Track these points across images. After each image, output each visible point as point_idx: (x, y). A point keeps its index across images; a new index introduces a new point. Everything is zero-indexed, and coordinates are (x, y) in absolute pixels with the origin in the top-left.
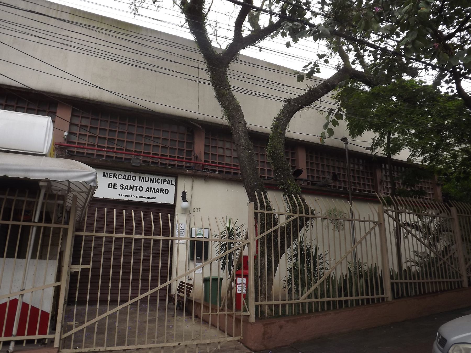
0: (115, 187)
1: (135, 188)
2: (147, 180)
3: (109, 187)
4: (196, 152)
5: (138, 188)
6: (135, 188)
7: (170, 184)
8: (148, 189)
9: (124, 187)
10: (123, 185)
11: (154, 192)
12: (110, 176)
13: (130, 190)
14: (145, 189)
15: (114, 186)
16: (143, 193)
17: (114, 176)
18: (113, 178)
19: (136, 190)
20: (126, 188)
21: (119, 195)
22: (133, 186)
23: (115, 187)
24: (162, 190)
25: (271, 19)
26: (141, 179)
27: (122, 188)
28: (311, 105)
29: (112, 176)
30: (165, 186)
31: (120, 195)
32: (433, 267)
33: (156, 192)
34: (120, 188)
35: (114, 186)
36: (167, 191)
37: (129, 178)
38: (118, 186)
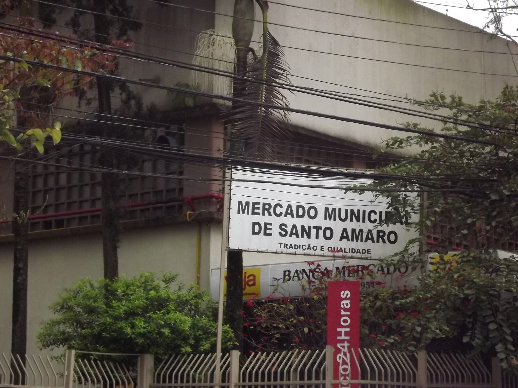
0: (268, 232)
1: (313, 232)
2: (343, 217)
3: (254, 233)
4: (429, 149)
5: (321, 232)
6: (313, 232)
7: (293, 216)
8: (372, 236)
9: (289, 229)
10: (286, 226)
11: (362, 241)
12: (256, 211)
13: (302, 237)
14: (337, 234)
15: (266, 230)
17: (264, 209)
18: (261, 213)
19: (317, 237)
20: (294, 232)
21: (281, 244)
22: (310, 227)
23: (268, 232)
24: (381, 234)
27: (283, 233)
28: (284, 105)
29: (258, 208)
31: (283, 246)
33: (366, 241)
34: (280, 234)
35: (266, 229)
37: (301, 213)
38: (275, 230)
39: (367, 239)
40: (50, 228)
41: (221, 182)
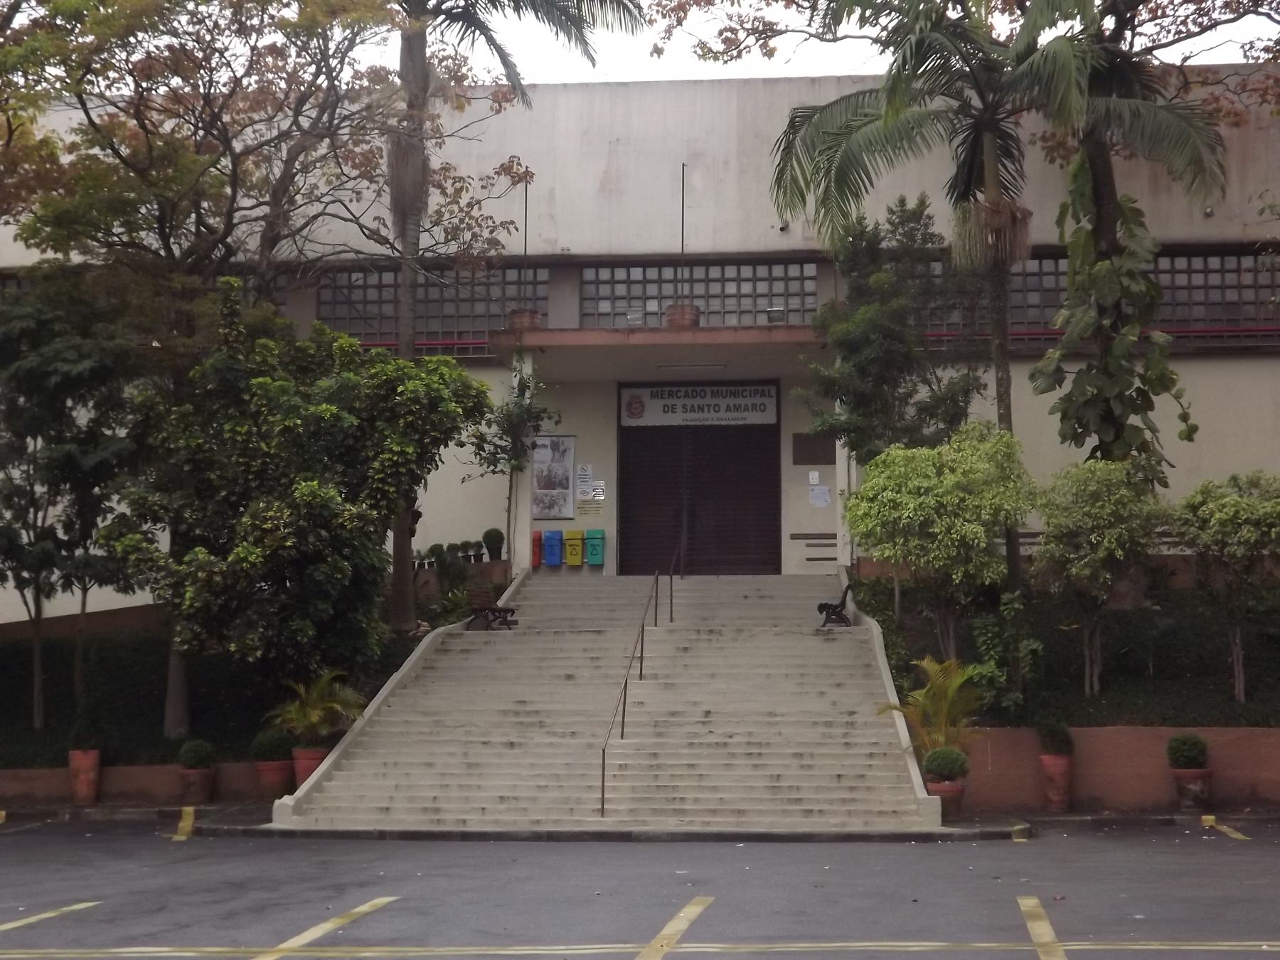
1: (706, 409)
5: (711, 408)
6: (706, 409)
9: (689, 408)
16: (722, 414)
25: (1114, 441)
26: (714, 395)
30: (758, 400)
32: (508, 810)
36: (762, 408)
39: (745, 410)
40: (753, 404)
41: (469, 287)
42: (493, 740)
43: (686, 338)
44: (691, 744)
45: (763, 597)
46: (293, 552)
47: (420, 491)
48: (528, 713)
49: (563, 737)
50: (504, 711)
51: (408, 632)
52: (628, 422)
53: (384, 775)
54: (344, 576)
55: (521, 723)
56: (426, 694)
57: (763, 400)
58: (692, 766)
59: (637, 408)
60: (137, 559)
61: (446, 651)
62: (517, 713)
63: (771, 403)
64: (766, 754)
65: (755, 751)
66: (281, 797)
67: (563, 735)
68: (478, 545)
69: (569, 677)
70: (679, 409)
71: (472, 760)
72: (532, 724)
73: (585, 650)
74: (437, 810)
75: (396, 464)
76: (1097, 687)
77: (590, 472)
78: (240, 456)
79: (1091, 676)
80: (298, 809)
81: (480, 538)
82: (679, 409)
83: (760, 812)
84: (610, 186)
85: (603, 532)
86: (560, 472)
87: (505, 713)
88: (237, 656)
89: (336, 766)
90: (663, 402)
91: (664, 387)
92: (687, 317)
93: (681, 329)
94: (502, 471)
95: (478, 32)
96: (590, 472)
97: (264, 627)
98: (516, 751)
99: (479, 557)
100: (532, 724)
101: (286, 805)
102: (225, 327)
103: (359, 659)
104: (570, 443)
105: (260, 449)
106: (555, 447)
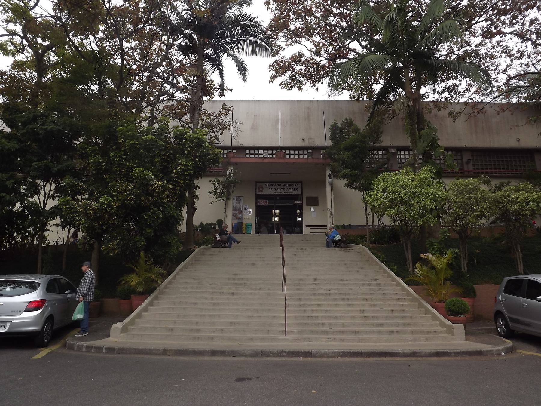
30: (296, 187)
42: (224, 291)
43: (282, 161)
44: (314, 294)
45: (308, 240)
46: (132, 202)
47: (195, 201)
48: (239, 279)
49: (256, 290)
50: (228, 278)
51: (191, 249)
52: (258, 193)
53: (173, 309)
54: (159, 218)
55: (236, 284)
56: (195, 270)
57: (297, 187)
58: (319, 305)
59: (261, 189)
60: (66, 208)
61: (204, 254)
62: (234, 279)
63: (300, 188)
64: (351, 299)
65: (347, 297)
66: (116, 323)
67: (256, 289)
68: (215, 224)
69: (253, 264)
70: (273, 189)
71: (215, 301)
72: (241, 284)
73: (257, 255)
74: (198, 331)
75: (183, 170)
76: (466, 269)
77: (247, 207)
78: (117, 167)
79: (464, 264)
80: (124, 330)
81: (216, 222)
82: (273, 189)
83: (367, 332)
84: (254, 127)
85: (251, 224)
86: (239, 207)
87: (229, 279)
88: (105, 252)
89: (151, 304)
90: (269, 187)
91: (270, 183)
92: (282, 155)
93: (280, 158)
94: (223, 200)
95: (217, 69)
96: (247, 207)
97: (120, 239)
98: (235, 297)
99: (215, 228)
100: (241, 284)
101: (117, 328)
102: (110, 108)
103: (167, 256)
104: (241, 198)
105: (127, 165)
106: (237, 199)
